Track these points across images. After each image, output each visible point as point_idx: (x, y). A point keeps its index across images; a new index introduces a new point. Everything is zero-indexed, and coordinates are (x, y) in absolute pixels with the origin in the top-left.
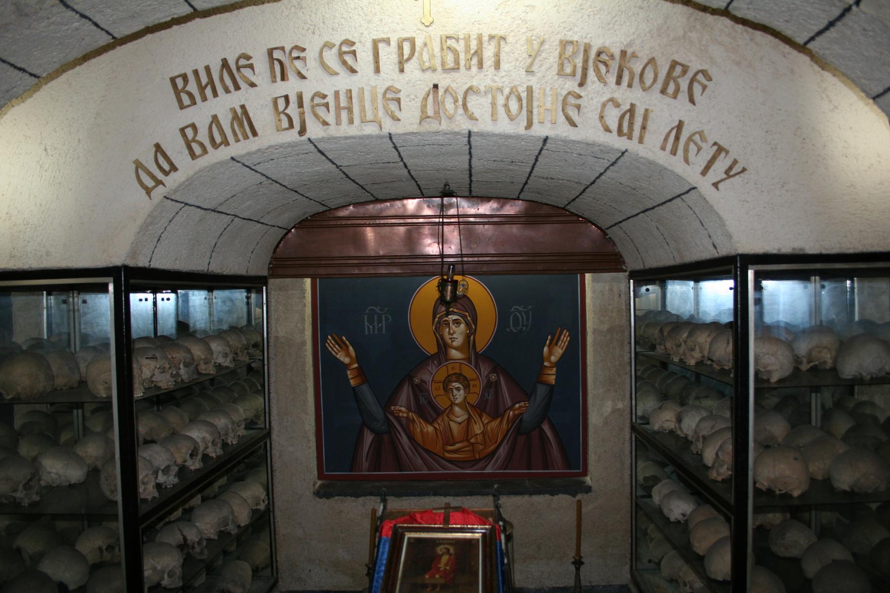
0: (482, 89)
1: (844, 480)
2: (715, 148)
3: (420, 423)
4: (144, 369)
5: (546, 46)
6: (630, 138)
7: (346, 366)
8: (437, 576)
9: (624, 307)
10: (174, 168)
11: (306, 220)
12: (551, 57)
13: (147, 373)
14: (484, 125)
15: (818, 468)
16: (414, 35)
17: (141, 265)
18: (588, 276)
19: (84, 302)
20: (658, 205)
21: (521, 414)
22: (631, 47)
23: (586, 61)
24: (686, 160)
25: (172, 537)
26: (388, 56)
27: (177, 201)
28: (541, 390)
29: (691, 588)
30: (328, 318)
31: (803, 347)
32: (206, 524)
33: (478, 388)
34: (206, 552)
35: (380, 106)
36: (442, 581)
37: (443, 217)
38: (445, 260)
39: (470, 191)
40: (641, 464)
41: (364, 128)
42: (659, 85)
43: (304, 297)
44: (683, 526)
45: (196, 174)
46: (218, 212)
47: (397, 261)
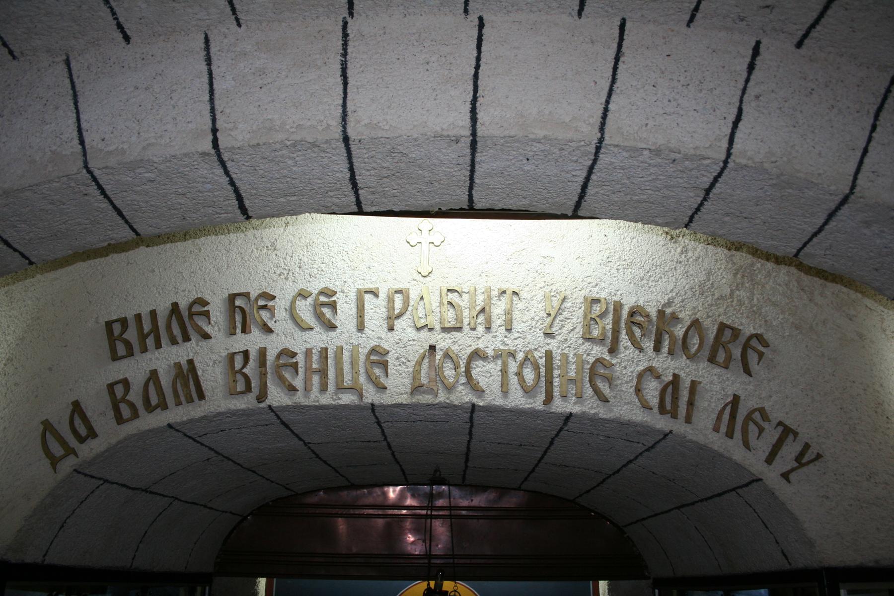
0: (490, 352)
2: (780, 429)
5: (567, 304)
6: (674, 416)
10: (92, 434)
12: (575, 318)
14: (493, 397)
16: (408, 286)
17: (29, 559)
20: (702, 501)
22: (670, 307)
23: (616, 322)
24: (746, 445)
26: (375, 310)
35: (362, 370)
37: (433, 508)
38: (433, 561)
39: (464, 478)
41: (340, 396)
42: (706, 352)
45: (119, 442)
46: (151, 492)
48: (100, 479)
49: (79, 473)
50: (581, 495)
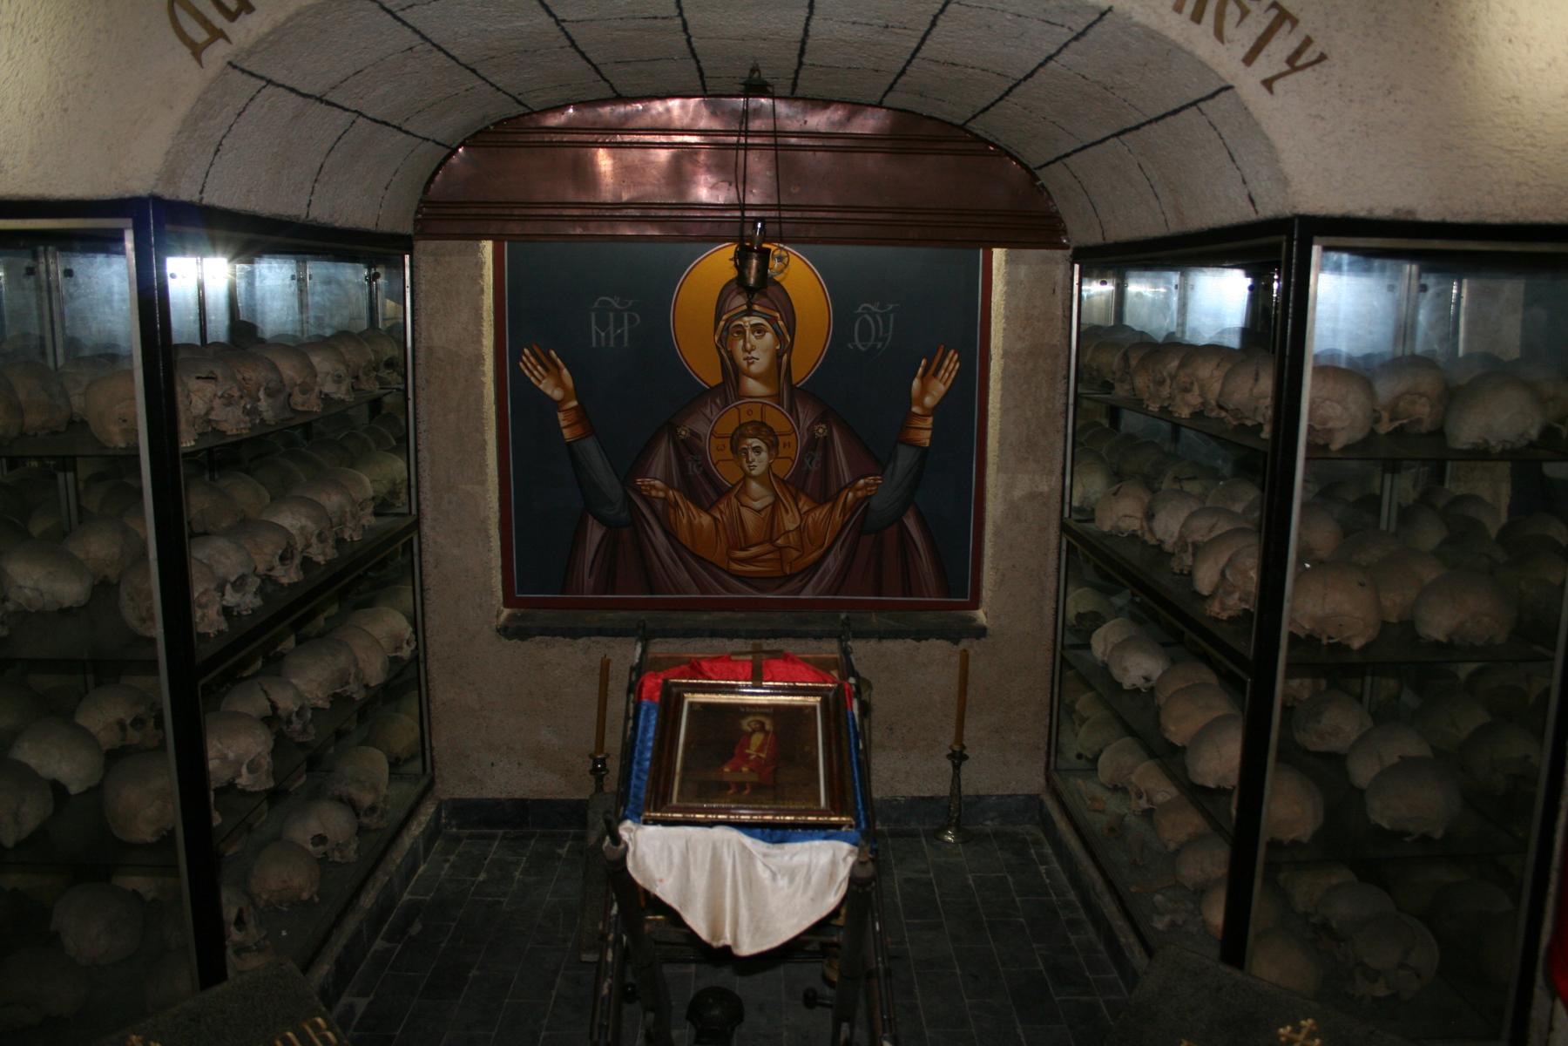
1: (1438, 623)
2: (1274, 13)
3: (688, 509)
4: (195, 398)
7: (556, 405)
8: (745, 769)
9: (1059, 313)
11: (485, 131)
13: (199, 406)
15: (1395, 601)
17: (184, 197)
18: (998, 254)
19: (69, 273)
20: (1150, 122)
21: (867, 497)
24: (1219, 34)
25: (250, 702)
27: (252, 74)
28: (905, 458)
29: (1149, 800)
30: (527, 316)
31: (1385, 389)
32: (307, 682)
33: (793, 448)
34: (312, 730)
36: (754, 778)
37: (747, 133)
38: (747, 214)
39: (795, 85)
40: (1074, 593)
43: (481, 276)
44: (1146, 696)
45: (290, 19)
46: (328, 103)
47: (653, 212)
48: (262, 78)
49: (235, 67)
50: (974, 117)
